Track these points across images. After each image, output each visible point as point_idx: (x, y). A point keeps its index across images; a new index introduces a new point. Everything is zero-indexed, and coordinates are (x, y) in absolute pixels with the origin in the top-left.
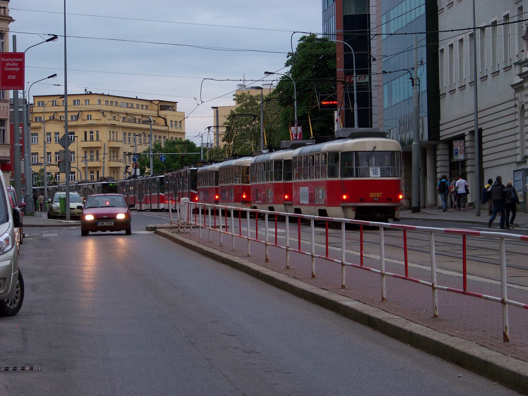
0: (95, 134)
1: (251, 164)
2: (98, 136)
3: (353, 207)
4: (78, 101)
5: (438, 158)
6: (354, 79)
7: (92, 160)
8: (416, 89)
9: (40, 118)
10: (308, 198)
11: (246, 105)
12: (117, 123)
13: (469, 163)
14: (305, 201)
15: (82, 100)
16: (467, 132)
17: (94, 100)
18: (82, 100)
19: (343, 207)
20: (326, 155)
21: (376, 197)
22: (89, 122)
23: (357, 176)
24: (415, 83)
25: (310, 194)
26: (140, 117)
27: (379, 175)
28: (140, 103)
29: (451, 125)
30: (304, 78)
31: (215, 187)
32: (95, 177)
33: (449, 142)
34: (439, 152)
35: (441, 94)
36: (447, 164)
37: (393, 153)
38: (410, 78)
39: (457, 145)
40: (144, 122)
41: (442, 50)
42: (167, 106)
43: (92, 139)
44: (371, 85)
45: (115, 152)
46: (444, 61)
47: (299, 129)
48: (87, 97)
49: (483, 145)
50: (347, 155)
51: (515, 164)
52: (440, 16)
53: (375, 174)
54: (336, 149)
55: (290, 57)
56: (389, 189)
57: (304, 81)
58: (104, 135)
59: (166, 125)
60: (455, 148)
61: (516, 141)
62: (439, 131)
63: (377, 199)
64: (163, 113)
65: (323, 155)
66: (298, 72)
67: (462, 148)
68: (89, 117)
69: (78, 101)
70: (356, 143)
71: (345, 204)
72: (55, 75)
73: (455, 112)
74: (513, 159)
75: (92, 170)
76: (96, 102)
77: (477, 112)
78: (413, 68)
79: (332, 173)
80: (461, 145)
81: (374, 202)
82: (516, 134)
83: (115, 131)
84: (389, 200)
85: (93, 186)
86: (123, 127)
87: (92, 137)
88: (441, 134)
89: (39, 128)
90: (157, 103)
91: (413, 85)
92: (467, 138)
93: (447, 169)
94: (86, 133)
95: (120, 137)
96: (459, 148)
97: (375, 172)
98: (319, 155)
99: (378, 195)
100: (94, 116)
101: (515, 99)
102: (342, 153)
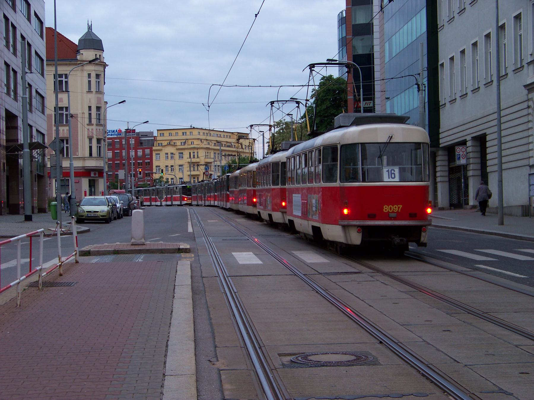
0: (196, 154)
1: (257, 168)
2: (198, 156)
4: (186, 133)
5: (438, 164)
6: (361, 105)
7: (194, 170)
8: (422, 94)
9: (161, 144)
10: (300, 208)
11: (282, 129)
12: (211, 147)
13: (471, 167)
14: (297, 212)
15: (188, 132)
16: (468, 138)
17: (195, 132)
18: (188, 132)
19: (344, 227)
20: (320, 151)
21: (393, 212)
23: (364, 181)
24: (421, 88)
25: (303, 204)
26: (225, 143)
27: (397, 179)
28: (226, 134)
29: (451, 132)
30: (324, 107)
31: (252, 188)
32: (196, 181)
33: (450, 150)
34: (438, 158)
35: (440, 104)
36: (447, 168)
37: (418, 145)
38: (416, 84)
39: (459, 151)
40: (228, 146)
41: (442, 65)
43: (194, 157)
44: (374, 109)
46: (444, 76)
48: (191, 130)
49: (487, 149)
50: (349, 148)
51: (528, 168)
52: (439, 34)
53: (391, 177)
54: (334, 141)
56: (413, 200)
57: (324, 110)
59: (242, 148)
60: (457, 153)
61: (529, 143)
62: (439, 139)
63: (394, 215)
65: (317, 152)
66: (319, 102)
67: (465, 153)
69: (186, 133)
70: (362, 131)
71: (346, 222)
72: (125, 101)
73: (456, 121)
74: (525, 162)
75: (194, 176)
76: (197, 133)
77: (500, 110)
78: (419, 74)
79: (329, 176)
80: (464, 150)
81: (390, 219)
82: (529, 136)
83: (209, 152)
84: (412, 217)
85: (176, 188)
86: (214, 149)
87: (194, 156)
88: (441, 141)
89: (161, 150)
90: (236, 134)
91: (419, 91)
92: (469, 144)
93: (447, 174)
94: (190, 153)
96: (461, 153)
97: (391, 174)
98: (311, 152)
99: (396, 208)
100: (196, 142)
101: (528, 100)
102: (342, 146)
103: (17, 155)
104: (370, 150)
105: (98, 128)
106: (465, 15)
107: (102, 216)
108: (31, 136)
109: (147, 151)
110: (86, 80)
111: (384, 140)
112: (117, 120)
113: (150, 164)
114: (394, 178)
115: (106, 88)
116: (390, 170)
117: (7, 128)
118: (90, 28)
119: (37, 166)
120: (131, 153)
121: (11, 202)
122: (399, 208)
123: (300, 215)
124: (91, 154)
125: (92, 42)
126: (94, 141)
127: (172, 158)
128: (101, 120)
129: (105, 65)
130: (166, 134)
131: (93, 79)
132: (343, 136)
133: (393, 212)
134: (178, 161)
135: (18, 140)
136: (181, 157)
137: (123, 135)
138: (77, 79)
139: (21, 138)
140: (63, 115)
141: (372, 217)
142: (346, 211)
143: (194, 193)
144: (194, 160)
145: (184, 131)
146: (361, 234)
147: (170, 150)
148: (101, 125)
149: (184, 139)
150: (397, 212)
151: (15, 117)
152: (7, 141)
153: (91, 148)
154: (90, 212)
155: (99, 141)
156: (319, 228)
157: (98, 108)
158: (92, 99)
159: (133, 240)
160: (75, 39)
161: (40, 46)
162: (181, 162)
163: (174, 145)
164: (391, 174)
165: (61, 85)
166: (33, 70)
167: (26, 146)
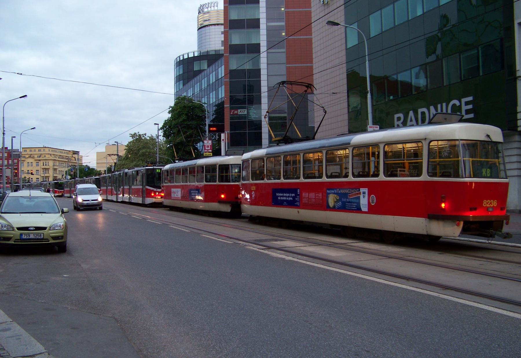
15: (42, 149)
17: (47, 150)
18: (42, 149)
22: (45, 158)
30: (181, 120)
42: (76, 153)
47: (210, 142)
55: (171, 109)
64: (74, 156)
68: (45, 156)
70: (461, 127)
72: (26, 96)
95: (57, 164)
100: (47, 156)
104: (414, 122)
107: (54, 238)
114: (450, 173)
119: (18, 336)
127: (32, 165)
130: (28, 150)
136: (37, 165)
143: (104, 186)
144: (45, 167)
145: (39, 149)
147: (30, 160)
149: (40, 154)
154: (26, 229)
162: (38, 168)
163: (33, 158)
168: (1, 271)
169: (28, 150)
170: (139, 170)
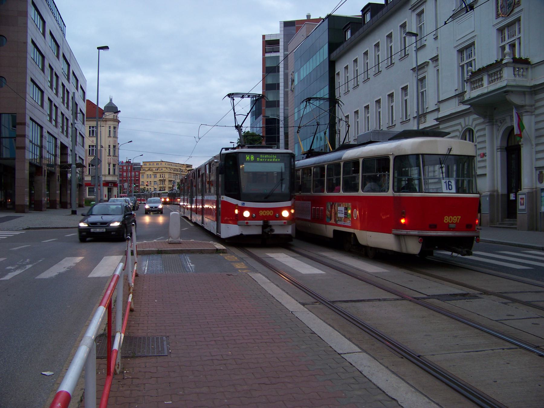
3: (419, 236)
15: (159, 163)
17: (163, 164)
18: (159, 163)
19: (398, 236)
21: (452, 223)
23: (419, 192)
27: (454, 190)
45: (171, 181)
58: (167, 176)
68: (162, 169)
70: (422, 143)
71: (404, 232)
81: (449, 229)
97: (449, 186)
99: (456, 219)
100: (164, 169)
103: (67, 171)
105: (114, 158)
106: (368, 83)
108: (76, 160)
109: (137, 173)
110: (108, 130)
111: (444, 152)
112: (124, 156)
113: (139, 180)
114: (451, 189)
115: (119, 136)
116: (447, 181)
117: (61, 154)
118: (111, 100)
120: (130, 173)
121: (63, 200)
122: (458, 218)
123: (309, 218)
124: (109, 173)
125: (112, 108)
126: (112, 165)
127: (151, 177)
128: (116, 155)
129: (119, 122)
130: (148, 164)
131: (112, 129)
132: (397, 147)
133: (452, 223)
134: (152, 179)
135: (67, 162)
137: (124, 164)
138: (104, 130)
139: (70, 160)
140: (94, 150)
141: (433, 227)
142: (403, 221)
144: (162, 179)
146: (421, 244)
147: (149, 173)
148: (116, 156)
149: (157, 167)
150: (456, 223)
151: (67, 147)
152: (61, 162)
153: (109, 169)
155: (114, 165)
156: (354, 234)
157: (114, 146)
158: (111, 141)
159: (170, 239)
160: (102, 106)
161: (83, 106)
163: (152, 170)
164: (449, 185)
165: (93, 133)
166: (78, 119)
167: (74, 166)
168: (2, 259)
169: (148, 164)
170: (191, 183)
